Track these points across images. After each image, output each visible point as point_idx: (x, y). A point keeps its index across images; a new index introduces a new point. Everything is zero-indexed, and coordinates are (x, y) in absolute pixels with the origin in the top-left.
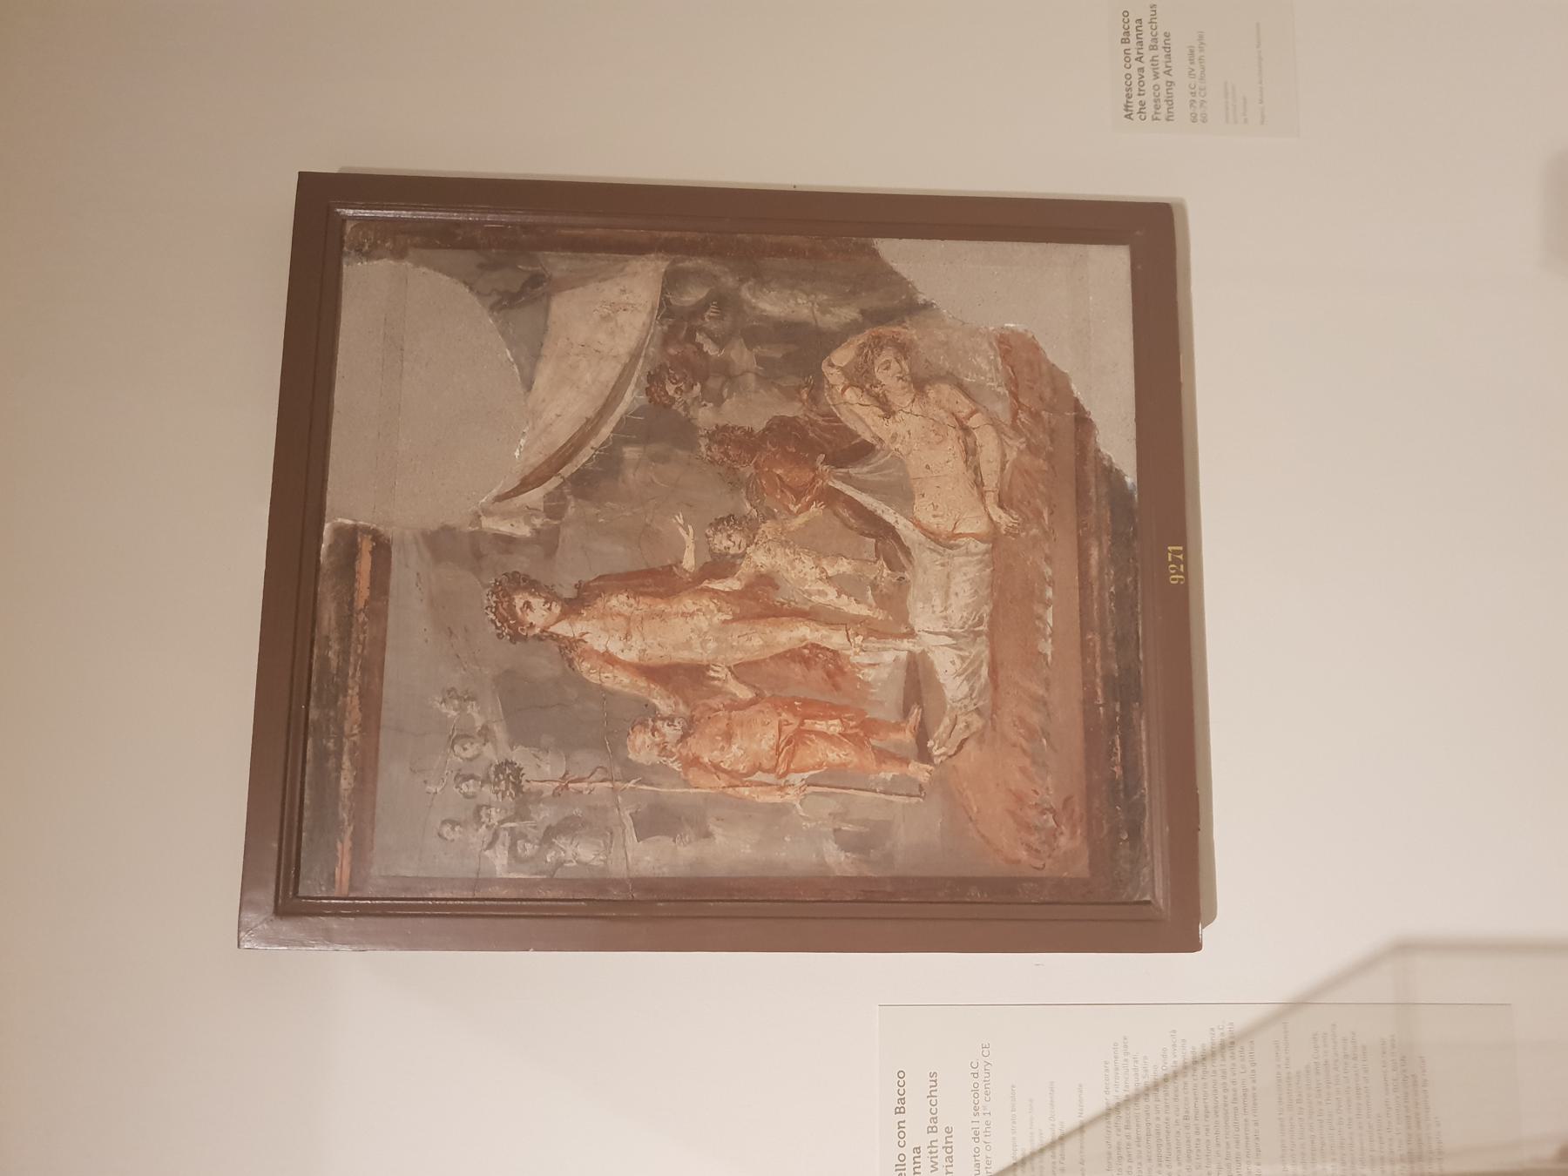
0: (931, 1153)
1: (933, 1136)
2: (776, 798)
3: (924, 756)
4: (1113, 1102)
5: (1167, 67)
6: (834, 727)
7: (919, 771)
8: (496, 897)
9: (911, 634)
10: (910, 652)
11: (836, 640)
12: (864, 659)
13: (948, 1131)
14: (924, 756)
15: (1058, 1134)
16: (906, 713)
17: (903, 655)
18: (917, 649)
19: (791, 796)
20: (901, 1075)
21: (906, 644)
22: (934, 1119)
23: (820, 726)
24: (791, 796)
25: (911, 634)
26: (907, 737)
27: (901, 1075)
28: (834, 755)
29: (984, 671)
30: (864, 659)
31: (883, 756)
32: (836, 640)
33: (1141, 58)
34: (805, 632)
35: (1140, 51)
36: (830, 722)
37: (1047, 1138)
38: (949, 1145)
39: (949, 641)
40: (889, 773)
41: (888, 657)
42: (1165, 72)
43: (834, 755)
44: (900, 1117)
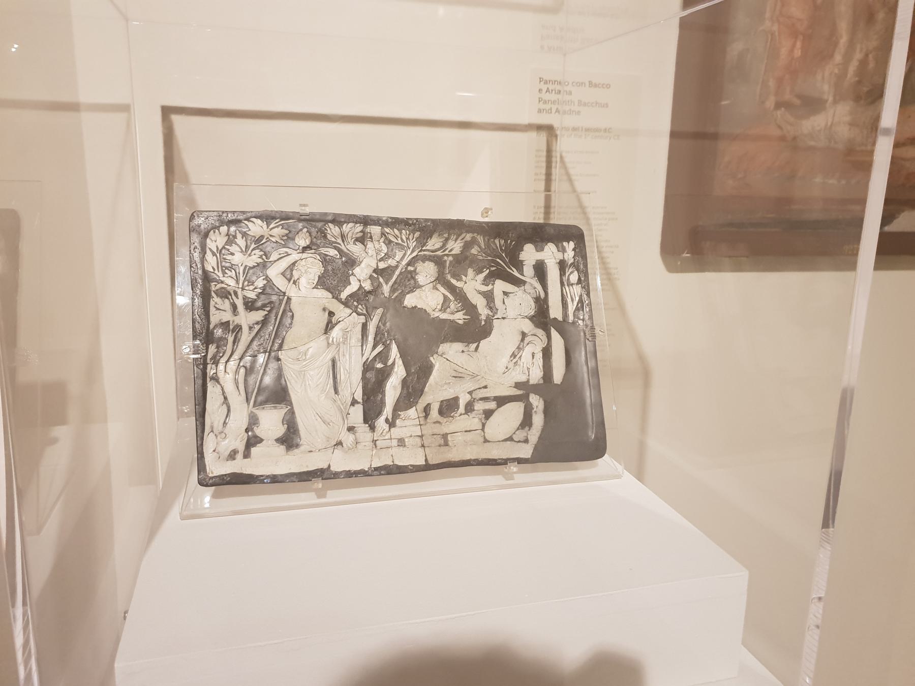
0: (568, 102)
1: (576, 103)
2: (768, 15)
3: (778, 105)
4: (588, 210)
5: (552, 91)
6: (798, 53)
7: (770, 103)
8: (544, 171)
9: (835, 102)
10: (827, 101)
11: (838, 58)
12: (827, 73)
13: (579, 113)
14: (778, 105)
15: (573, 178)
16: (799, 97)
17: (825, 97)
18: (828, 105)
19: (768, 24)
20: (608, 86)
21: (831, 99)
22: (585, 104)
23: (799, 44)
24: (768, 24)
25: (835, 102)
26: (787, 96)
27: (608, 86)
28: (784, 51)
29: (812, 143)
30: (827, 73)
31: (780, 81)
32: (838, 58)
33: (549, 92)
34: (844, 40)
35: (554, 92)
36: (800, 51)
37: (571, 171)
38: (572, 113)
39: (829, 124)
40: (772, 83)
41: (826, 87)
42: (548, 88)
43: (784, 51)
44: (587, 84)
